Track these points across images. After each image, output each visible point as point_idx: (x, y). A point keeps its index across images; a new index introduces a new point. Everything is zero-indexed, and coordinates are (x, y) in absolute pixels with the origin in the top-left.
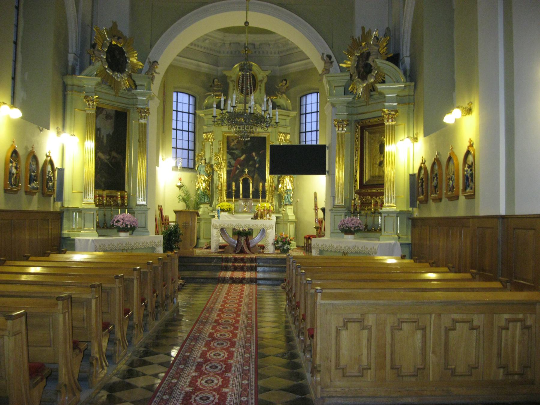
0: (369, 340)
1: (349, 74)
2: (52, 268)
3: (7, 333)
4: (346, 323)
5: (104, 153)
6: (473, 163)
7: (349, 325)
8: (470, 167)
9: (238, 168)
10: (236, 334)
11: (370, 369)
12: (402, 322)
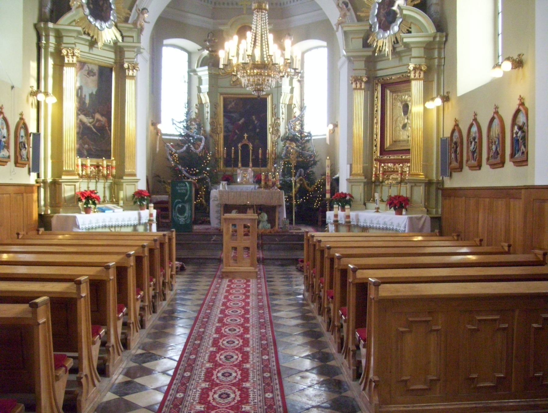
2: (474, 247)
5: (86, 115)
6: (526, 124)
8: (520, 128)
9: (236, 134)
10: (221, 314)
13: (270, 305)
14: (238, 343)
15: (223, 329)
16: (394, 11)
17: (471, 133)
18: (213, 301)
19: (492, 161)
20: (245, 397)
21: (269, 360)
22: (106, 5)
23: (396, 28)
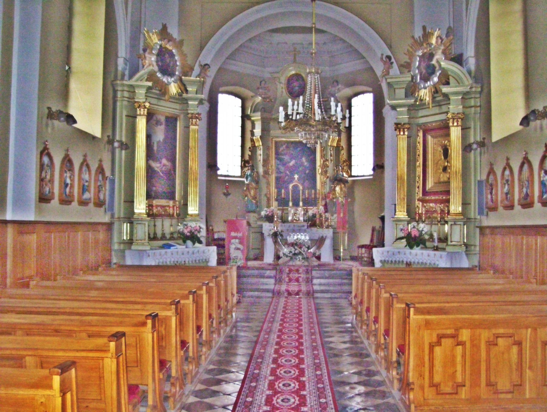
0: (464, 356)
1: (410, 76)
3: (110, 355)
4: (440, 337)
7: (443, 340)
9: (288, 175)
11: (464, 386)
12: (497, 336)
13: (324, 343)
14: (295, 361)
15: (278, 371)
16: (433, 65)
17: (505, 176)
18: (276, 310)
19: (523, 202)
20: (303, 401)
21: (321, 374)
22: (172, 63)
23: (436, 79)
